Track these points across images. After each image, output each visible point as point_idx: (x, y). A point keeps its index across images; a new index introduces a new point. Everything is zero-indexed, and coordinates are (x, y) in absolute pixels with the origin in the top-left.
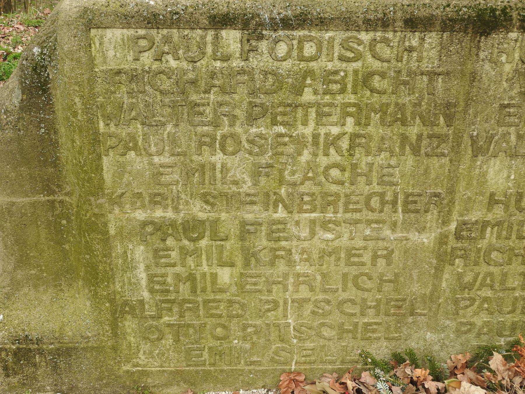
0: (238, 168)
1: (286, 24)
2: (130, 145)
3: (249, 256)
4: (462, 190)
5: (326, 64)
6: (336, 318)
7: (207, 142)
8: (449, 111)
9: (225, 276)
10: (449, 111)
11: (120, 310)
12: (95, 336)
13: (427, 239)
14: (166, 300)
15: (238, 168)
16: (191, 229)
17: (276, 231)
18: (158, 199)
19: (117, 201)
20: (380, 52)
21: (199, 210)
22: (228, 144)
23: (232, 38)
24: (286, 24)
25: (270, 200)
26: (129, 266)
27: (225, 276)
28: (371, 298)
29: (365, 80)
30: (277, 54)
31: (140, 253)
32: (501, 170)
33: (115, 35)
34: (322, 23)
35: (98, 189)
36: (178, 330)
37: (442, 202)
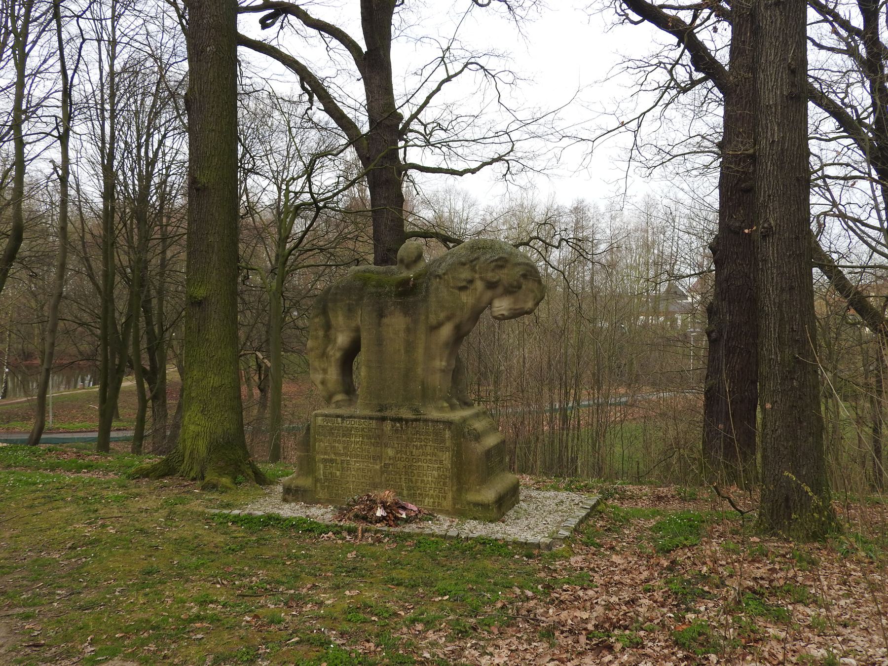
0: (340, 447)
1: (349, 417)
2: (321, 441)
3: (343, 468)
4: (384, 456)
5: (356, 426)
6: (361, 487)
7: (335, 441)
8: (379, 437)
9: (338, 473)
10: (379, 437)
11: (317, 480)
12: (670, 346)
13: (378, 467)
14: (326, 480)
15: (340, 447)
16: (332, 461)
17: (348, 462)
18: (325, 453)
19: (318, 453)
20: (365, 424)
21: (333, 457)
22: (339, 442)
23: (339, 419)
24: (349, 417)
25: (347, 455)
26: (319, 469)
27: (338, 473)
28: (368, 482)
29: (363, 429)
30: (347, 423)
31: (322, 466)
32: (583, 288)
33: (320, 418)
34: (355, 418)
35: (315, 450)
36: (328, 487)
37: (380, 457)
